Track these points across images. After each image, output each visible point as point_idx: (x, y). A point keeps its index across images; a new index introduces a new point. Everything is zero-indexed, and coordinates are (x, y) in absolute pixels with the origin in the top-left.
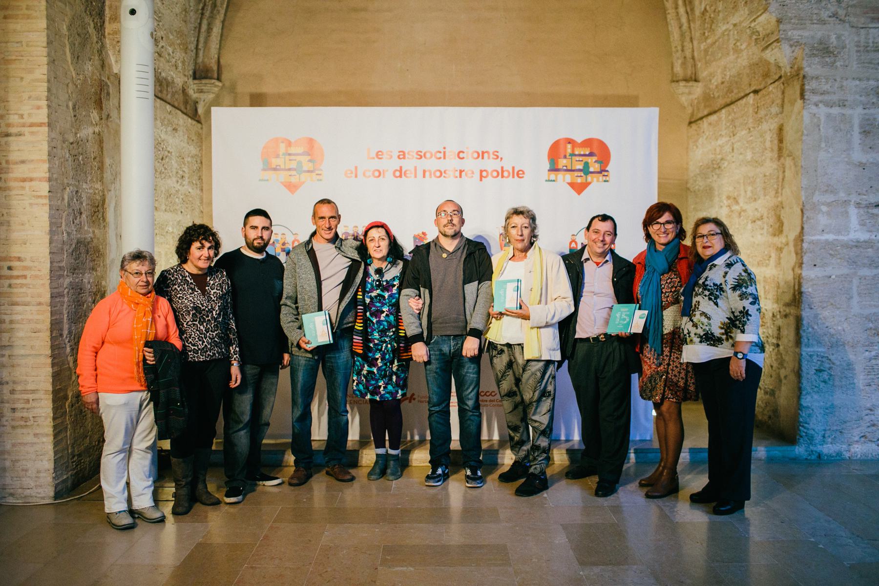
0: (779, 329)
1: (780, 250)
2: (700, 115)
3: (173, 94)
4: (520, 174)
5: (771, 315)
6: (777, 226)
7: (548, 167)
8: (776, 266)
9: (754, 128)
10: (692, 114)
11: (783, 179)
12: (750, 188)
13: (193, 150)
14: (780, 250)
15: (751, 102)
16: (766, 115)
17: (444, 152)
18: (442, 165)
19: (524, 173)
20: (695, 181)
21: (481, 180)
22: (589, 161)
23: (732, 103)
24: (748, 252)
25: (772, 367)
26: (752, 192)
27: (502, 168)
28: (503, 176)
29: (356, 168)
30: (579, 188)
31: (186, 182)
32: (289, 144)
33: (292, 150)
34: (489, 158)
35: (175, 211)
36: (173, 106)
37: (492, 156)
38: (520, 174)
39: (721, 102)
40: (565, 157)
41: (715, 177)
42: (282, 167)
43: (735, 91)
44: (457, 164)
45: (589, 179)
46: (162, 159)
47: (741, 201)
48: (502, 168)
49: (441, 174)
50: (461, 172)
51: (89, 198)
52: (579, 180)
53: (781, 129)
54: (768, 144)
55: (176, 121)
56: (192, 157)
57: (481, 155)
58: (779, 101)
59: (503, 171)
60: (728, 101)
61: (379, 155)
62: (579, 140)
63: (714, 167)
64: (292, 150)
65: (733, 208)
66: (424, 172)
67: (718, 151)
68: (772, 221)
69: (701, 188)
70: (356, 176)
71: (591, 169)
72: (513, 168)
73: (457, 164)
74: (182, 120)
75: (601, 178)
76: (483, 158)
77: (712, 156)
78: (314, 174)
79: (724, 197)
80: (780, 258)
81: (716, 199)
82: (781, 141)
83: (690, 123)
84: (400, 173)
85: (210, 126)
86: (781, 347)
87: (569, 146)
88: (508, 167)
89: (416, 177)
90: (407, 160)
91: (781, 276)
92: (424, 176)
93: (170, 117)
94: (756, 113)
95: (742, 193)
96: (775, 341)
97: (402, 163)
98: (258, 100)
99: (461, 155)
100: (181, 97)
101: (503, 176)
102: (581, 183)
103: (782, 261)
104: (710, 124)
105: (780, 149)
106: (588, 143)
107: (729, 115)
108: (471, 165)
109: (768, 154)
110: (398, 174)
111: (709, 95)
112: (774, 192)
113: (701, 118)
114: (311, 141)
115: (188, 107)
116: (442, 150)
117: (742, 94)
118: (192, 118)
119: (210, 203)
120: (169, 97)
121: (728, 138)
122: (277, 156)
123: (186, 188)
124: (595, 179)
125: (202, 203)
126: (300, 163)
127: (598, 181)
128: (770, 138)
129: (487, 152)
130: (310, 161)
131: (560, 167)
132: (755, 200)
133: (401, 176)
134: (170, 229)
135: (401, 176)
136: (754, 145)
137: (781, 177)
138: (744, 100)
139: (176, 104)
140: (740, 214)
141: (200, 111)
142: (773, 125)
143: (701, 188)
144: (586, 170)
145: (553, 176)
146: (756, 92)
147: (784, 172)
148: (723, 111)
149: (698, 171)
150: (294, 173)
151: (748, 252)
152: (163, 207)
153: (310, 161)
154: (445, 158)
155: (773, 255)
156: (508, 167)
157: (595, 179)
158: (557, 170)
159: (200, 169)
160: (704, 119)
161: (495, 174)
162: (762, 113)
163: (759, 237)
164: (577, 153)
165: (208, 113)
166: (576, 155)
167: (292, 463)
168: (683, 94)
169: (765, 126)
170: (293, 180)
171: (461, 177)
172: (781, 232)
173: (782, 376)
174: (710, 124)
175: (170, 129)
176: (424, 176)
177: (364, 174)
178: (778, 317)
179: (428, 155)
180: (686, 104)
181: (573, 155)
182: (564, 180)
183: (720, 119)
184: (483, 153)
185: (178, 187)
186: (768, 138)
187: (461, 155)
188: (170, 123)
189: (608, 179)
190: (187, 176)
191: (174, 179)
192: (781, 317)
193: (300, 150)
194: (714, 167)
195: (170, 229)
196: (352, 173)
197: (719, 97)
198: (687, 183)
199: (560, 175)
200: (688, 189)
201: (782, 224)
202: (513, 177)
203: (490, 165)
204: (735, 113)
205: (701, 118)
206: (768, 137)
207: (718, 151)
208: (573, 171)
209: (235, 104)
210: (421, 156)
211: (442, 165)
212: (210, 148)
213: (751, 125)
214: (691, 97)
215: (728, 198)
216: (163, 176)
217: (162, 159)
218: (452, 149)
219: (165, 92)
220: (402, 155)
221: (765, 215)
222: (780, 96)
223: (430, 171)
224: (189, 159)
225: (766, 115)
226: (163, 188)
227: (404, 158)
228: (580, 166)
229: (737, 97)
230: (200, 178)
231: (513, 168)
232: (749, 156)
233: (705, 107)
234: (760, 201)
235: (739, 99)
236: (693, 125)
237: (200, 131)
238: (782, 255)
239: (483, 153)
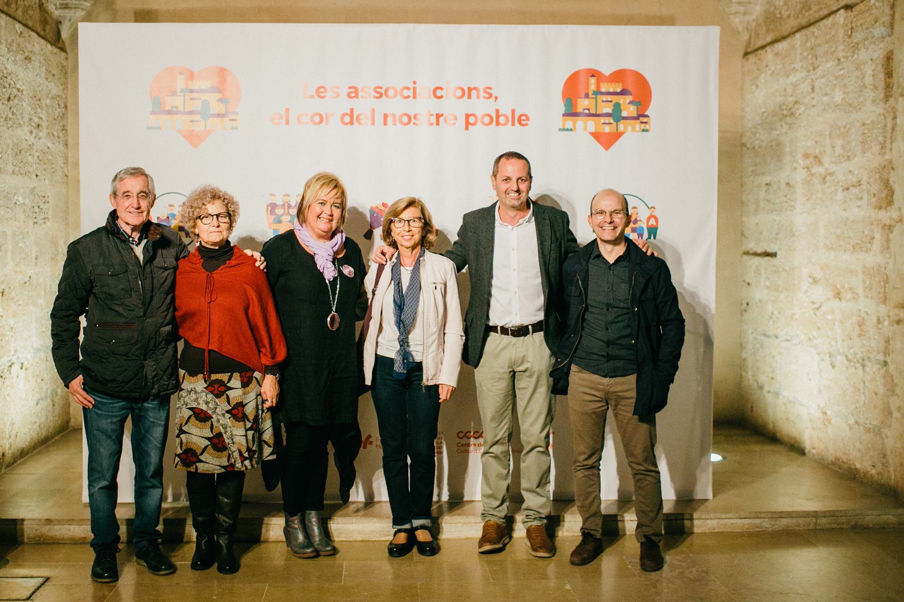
0: (887, 341)
1: (889, 228)
2: (761, 43)
3: (25, 12)
5: (875, 320)
6: (884, 195)
7: (562, 110)
8: (882, 252)
9: (846, 57)
10: (749, 43)
11: (893, 129)
12: (839, 143)
13: (54, 88)
14: (889, 228)
15: (842, 21)
16: (866, 39)
17: (415, 89)
18: (410, 107)
19: (528, 119)
20: (755, 134)
21: (467, 129)
22: (621, 102)
23: (810, 25)
24: (838, 231)
25: (876, 394)
26: (843, 147)
27: (497, 111)
28: (498, 124)
29: (287, 110)
30: (607, 140)
31: (43, 134)
32: (191, 76)
33: (197, 85)
34: (478, 97)
35: (27, 173)
36: (26, 26)
37: (482, 94)
39: (793, 23)
40: (587, 96)
41: (786, 127)
42: (181, 109)
43: (815, 8)
44: (434, 106)
45: (621, 127)
46: (9, 99)
47: (826, 160)
48: (497, 111)
49: (410, 119)
50: (438, 116)
51: (715, 392)
52: (607, 129)
53: (889, 58)
54: (869, 80)
55: (29, 47)
56: (52, 98)
57: (468, 92)
58: (886, 19)
59: (498, 116)
60: (804, 22)
61: (320, 92)
62: (607, 71)
63: (786, 114)
64: (197, 85)
65: (813, 171)
66: (386, 116)
67: (789, 91)
68: (876, 187)
69: (764, 144)
70: (287, 123)
71: (624, 114)
72: (513, 111)
73: (434, 106)
74: (38, 46)
75: (638, 126)
76: (469, 97)
77: (780, 99)
78: (226, 119)
79: (799, 156)
80: (888, 241)
81: (788, 158)
82: (889, 74)
83: (746, 54)
84: (351, 118)
85: (77, 55)
86: (891, 367)
87: (593, 81)
88: (505, 110)
89: (373, 124)
90: (360, 99)
91: (890, 266)
92: (385, 124)
93: (21, 40)
94: (850, 37)
95: (828, 150)
96: (881, 357)
97: (353, 103)
98: (144, 16)
99: (439, 93)
100: (37, 14)
101: (498, 124)
102: (610, 134)
103: (892, 245)
104: (777, 54)
105: (888, 87)
106: (619, 76)
107: (807, 40)
108: (453, 107)
109: (869, 94)
110: (347, 119)
111: (775, 15)
112: (879, 148)
113: (763, 47)
114: (222, 73)
115: (48, 28)
116: (411, 86)
117: (826, 12)
118: (52, 44)
119: (77, 165)
120: (20, 12)
121: (805, 73)
122: (174, 93)
123: (43, 141)
124: (630, 128)
125: (66, 162)
126: (206, 104)
127: (634, 130)
128: (871, 72)
129: (475, 88)
130: (220, 100)
131: (580, 110)
132: (849, 158)
133: (351, 123)
134: (20, 199)
135: (351, 123)
136: (846, 81)
137: (890, 125)
138: (831, 19)
139: (30, 23)
140: (824, 179)
141: (65, 34)
142: (878, 52)
143: (764, 144)
144: (616, 115)
145: (569, 123)
146: (848, 7)
147: (895, 118)
148: (798, 35)
149: (758, 120)
150: (197, 117)
151: (838, 231)
152: (10, 168)
153: (220, 100)
154: (415, 97)
155: (878, 236)
156: (505, 110)
157: (630, 128)
158: (575, 114)
159: (63, 116)
160: (768, 49)
161: (487, 120)
162: (859, 36)
163: (856, 210)
164: (603, 90)
165: (74, 36)
166: (602, 93)
167: (195, 539)
168: (736, 13)
169: (863, 55)
170: (198, 128)
171: (438, 123)
172: (890, 203)
173: (893, 408)
174: (777, 54)
175: (20, 57)
176: (385, 124)
177: (299, 120)
178: (886, 323)
179: (391, 93)
180: (740, 28)
181: (598, 92)
182: (585, 130)
183: (793, 47)
184: (470, 89)
185: (31, 139)
186: (870, 72)
187: (439, 93)
188: (21, 49)
189: (647, 127)
190: (44, 124)
191: (26, 129)
192: (891, 324)
193: (206, 84)
194: (786, 114)
195: (20, 199)
196: (281, 117)
197: (789, 16)
198: (741, 136)
199: (580, 122)
200: (744, 145)
201: (892, 192)
202: (513, 124)
203: (481, 106)
204: (816, 37)
205: (763, 47)
206: (869, 70)
207: (789, 91)
208: (599, 115)
209: (114, 19)
210: (380, 93)
211: (410, 107)
212: (76, 86)
213: (840, 54)
214: (747, 18)
215: (806, 156)
216: (10, 123)
217: (9, 99)
218: (425, 86)
219: (13, 5)
220: (354, 93)
221: (865, 178)
222: (887, 11)
223: (394, 116)
224: (48, 101)
225: (866, 39)
226: (9, 141)
227: (356, 96)
228: (608, 109)
229: (817, 16)
230: (64, 129)
231: (513, 111)
232: (838, 97)
233: (768, 31)
234: (856, 160)
235: (822, 19)
236: (752, 58)
237: (64, 63)
238: (891, 236)
239: (470, 89)
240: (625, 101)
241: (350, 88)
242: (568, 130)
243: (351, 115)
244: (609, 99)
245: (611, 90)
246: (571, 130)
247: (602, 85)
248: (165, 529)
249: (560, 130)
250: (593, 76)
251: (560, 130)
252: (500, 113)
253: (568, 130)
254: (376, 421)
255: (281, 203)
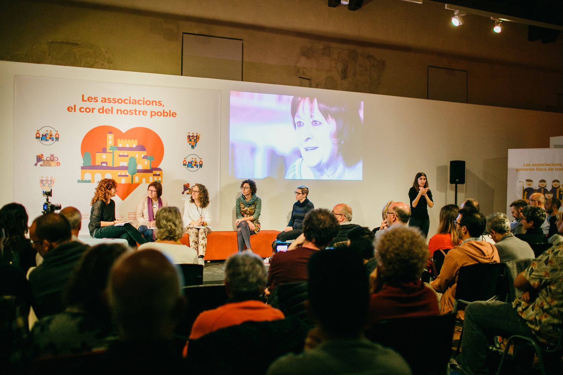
4: (174, 115)
7: (81, 163)
22: (137, 156)
28: (164, 115)
29: (75, 106)
38: (174, 115)
59: (164, 113)
66: (118, 110)
72: (170, 111)
92: (117, 113)
110: (101, 111)
135: (103, 112)
164: (120, 145)
176: (117, 113)
184: (153, 102)
196: (72, 109)
223: (121, 110)
231: (170, 111)
239: (153, 102)
240: (140, 156)
242: (86, 181)
243: (103, 109)
244: (126, 154)
245: (127, 146)
246: (89, 182)
247: (119, 140)
249: (79, 181)
250: (110, 133)
251: (79, 181)
253: (86, 181)
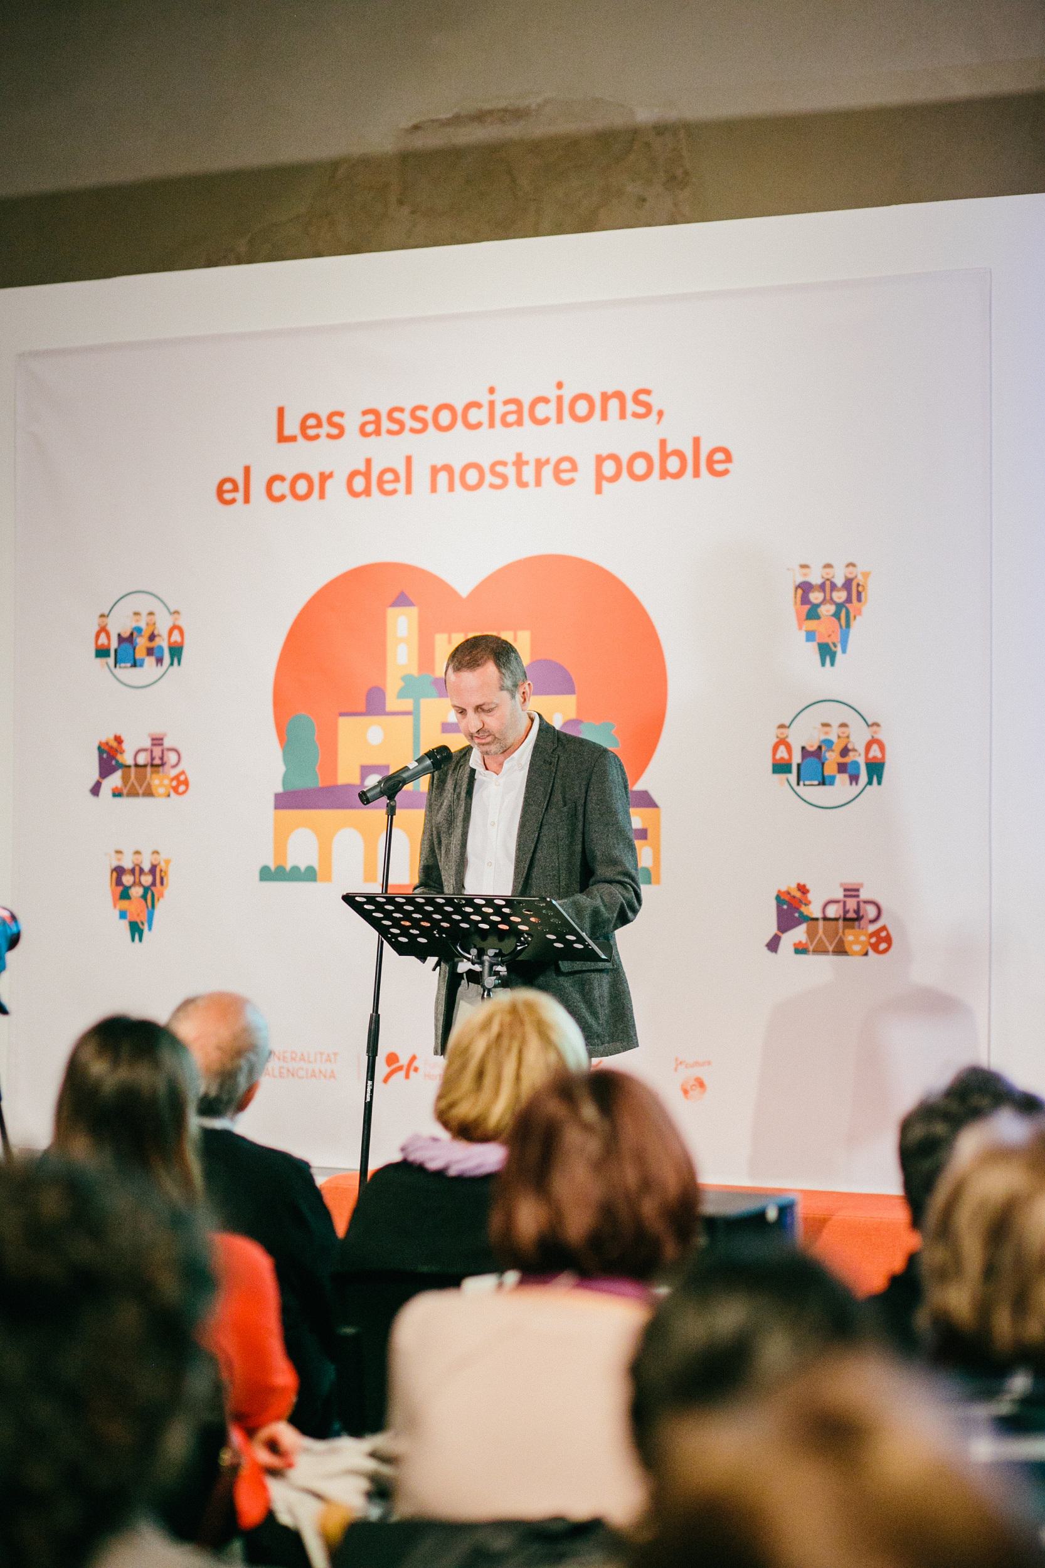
19: (729, 459)
21: (599, 490)
27: (663, 443)
48: (663, 443)
59: (664, 456)
66: (435, 471)
72: (697, 441)
76: (604, 417)
92: (434, 489)
110: (359, 483)
176: (434, 489)
184: (605, 398)
202: (696, 474)
231: (697, 441)
239: (605, 398)
241: (365, 413)
248: (346, 1338)
252: (669, 449)
254: (821, 1189)
255: (819, 581)
